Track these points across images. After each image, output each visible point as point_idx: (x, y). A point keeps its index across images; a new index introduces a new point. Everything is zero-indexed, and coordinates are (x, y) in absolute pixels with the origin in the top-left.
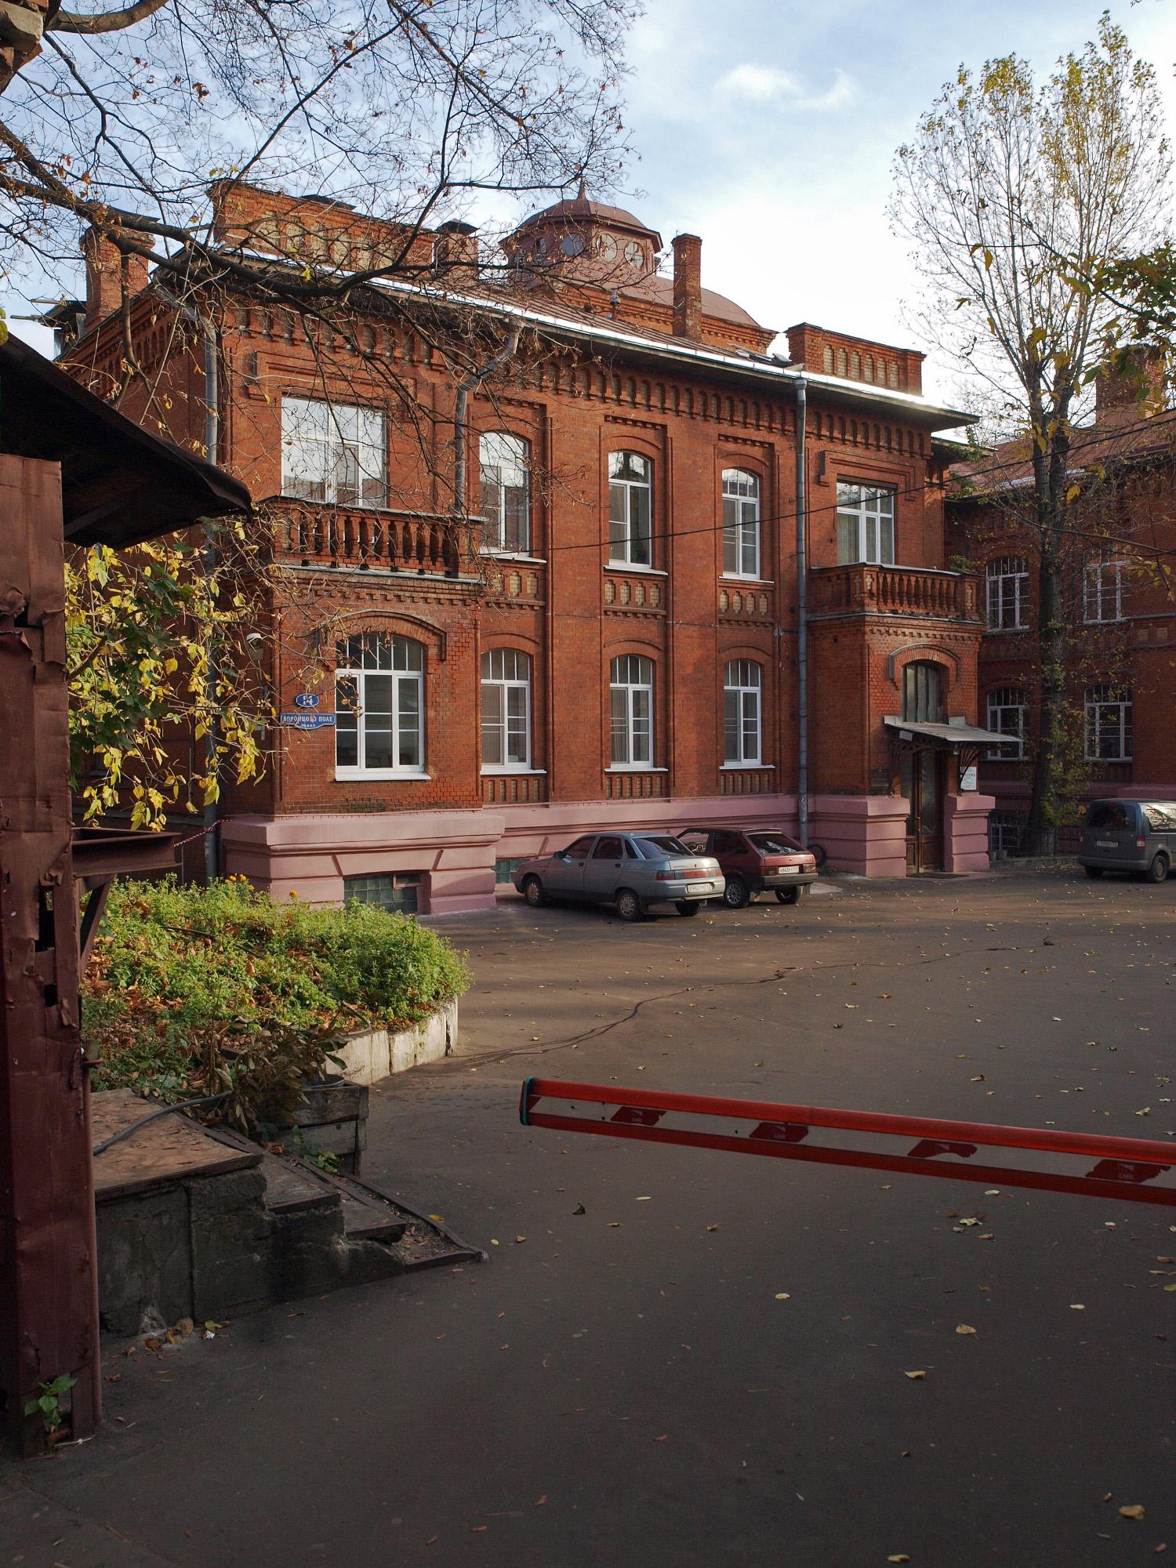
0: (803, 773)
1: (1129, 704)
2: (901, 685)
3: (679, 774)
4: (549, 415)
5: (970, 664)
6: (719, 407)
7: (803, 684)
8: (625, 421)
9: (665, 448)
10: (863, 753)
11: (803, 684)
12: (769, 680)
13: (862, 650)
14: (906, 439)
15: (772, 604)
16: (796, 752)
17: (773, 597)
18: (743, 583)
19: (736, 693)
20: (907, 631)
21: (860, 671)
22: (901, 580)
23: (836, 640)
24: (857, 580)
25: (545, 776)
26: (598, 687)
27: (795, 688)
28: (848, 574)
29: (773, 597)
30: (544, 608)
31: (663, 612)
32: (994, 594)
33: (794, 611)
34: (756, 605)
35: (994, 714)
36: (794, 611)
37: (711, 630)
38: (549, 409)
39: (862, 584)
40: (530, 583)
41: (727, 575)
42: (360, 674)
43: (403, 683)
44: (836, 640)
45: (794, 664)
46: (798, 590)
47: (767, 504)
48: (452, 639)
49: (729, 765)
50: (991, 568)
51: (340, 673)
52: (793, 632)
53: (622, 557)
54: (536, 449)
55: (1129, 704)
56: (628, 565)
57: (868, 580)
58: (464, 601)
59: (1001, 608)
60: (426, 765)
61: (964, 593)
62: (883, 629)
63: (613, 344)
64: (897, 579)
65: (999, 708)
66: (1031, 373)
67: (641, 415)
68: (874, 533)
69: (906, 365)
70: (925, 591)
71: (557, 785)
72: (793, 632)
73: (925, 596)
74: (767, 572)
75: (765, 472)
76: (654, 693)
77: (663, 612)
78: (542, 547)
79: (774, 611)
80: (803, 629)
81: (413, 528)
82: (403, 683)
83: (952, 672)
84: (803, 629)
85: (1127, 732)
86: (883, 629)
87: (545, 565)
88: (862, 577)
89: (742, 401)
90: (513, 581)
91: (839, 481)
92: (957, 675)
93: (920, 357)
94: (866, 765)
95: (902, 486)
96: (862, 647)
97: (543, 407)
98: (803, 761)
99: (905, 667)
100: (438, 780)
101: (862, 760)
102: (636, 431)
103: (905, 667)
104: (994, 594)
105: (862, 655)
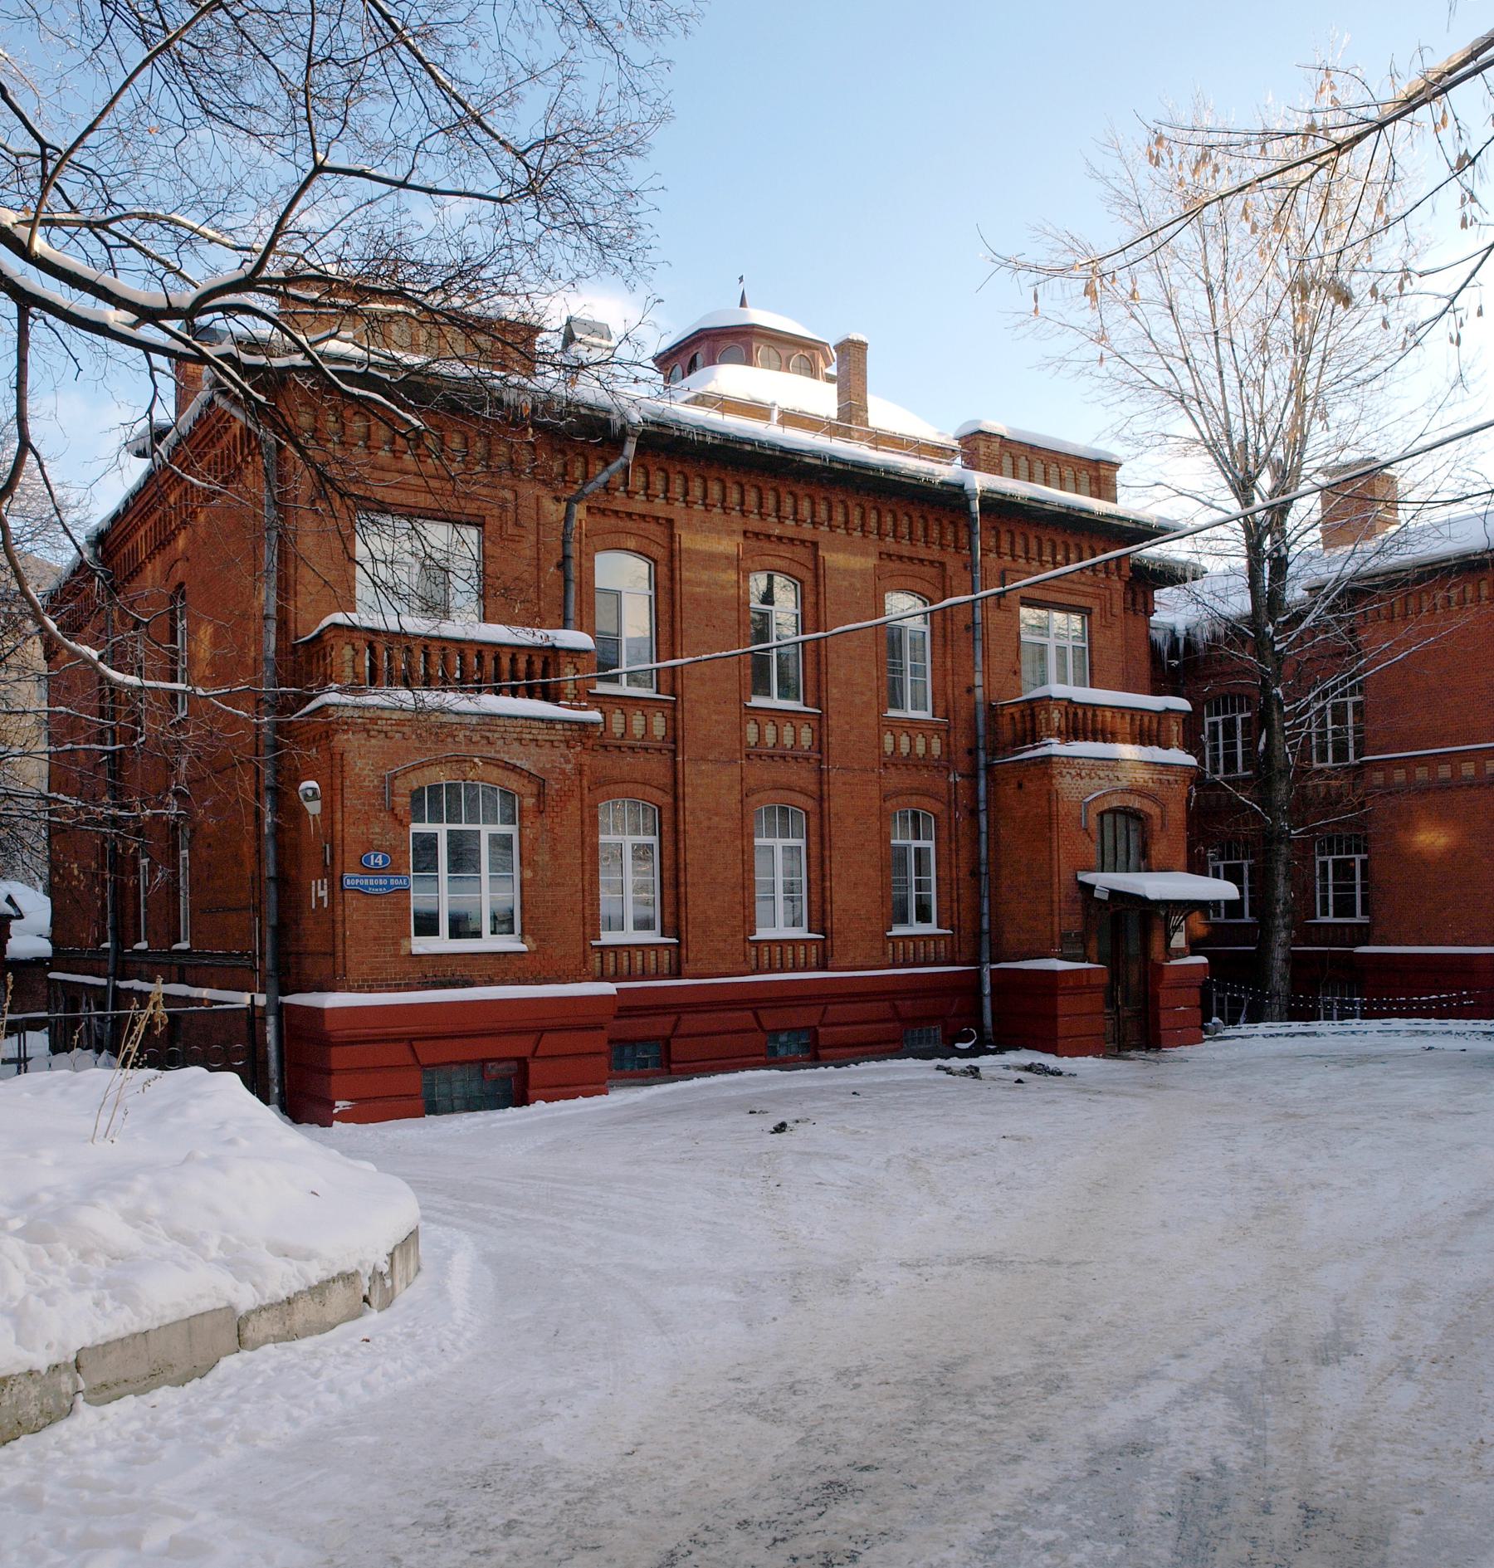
0: (986, 938)
1: (1365, 856)
2: (1096, 837)
3: (837, 942)
4: (677, 531)
5: (1177, 812)
6: (1012, 543)
7: (984, 836)
8: (900, 558)
9: (816, 568)
10: (1051, 914)
11: (984, 836)
12: (944, 834)
13: (1051, 795)
14: (1115, 562)
15: (946, 745)
16: (980, 915)
17: (948, 737)
18: (911, 720)
19: (905, 848)
20: (1102, 774)
21: (1049, 820)
22: (1094, 715)
23: (1020, 786)
24: (1043, 716)
25: (678, 946)
26: (738, 842)
27: (976, 841)
28: (1032, 709)
29: (948, 737)
30: (674, 753)
31: (818, 756)
32: (1214, 736)
33: (972, 752)
34: (928, 746)
35: (1324, 865)
36: (972, 752)
37: (874, 776)
38: (677, 524)
39: (1048, 720)
40: (806, 735)
41: (892, 713)
42: (441, 830)
43: (494, 839)
44: (1020, 786)
45: (974, 813)
46: (976, 729)
47: (938, 632)
48: (553, 786)
49: (898, 930)
50: (1209, 708)
51: (416, 828)
52: (973, 776)
53: (768, 694)
54: (663, 570)
55: (1365, 856)
56: (774, 702)
57: (1056, 715)
58: (567, 742)
59: (1221, 752)
60: (522, 934)
61: (1169, 730)
62: (1073, 772)
63: (1115, 522)
64: (1090, 714)
65: (1330, 859)
66: (1243, 488)
67: (789, 529)
68: (1065, 666)
69: (1098, 473)
70: (1085, 724)
71: (691, 956)
72: (973, 776)
73: (1103, 731)
74: (940, 710)
75: (808, 576)
76: (808, 848)
77: (818, 756)
78: (817, 696)
79: (949, 753)
80: (982, 773)
81: (1146, 719)
82: (494, 839)
83: (1157, 822)
84: (982, 773)
85: (1364, 887)
86: (1073, 772)
87: (675, 702)
88: (1047, 711)
89: (907, 514)
90: (638, 722)
91: (1022, 604)
92: (1163, 824)
93: (1117, 465)
94: (1056, 929)
95: (1096, 610)
96: (1049, 793)
97: (670, 522)
98: (985, 926)
99: (1101, 815)
100: (536, 952)
101: (1052, 923)
102: (916, 567)
103: (1101, 815)
104: (1214, 736)
105: (1049, 801)
